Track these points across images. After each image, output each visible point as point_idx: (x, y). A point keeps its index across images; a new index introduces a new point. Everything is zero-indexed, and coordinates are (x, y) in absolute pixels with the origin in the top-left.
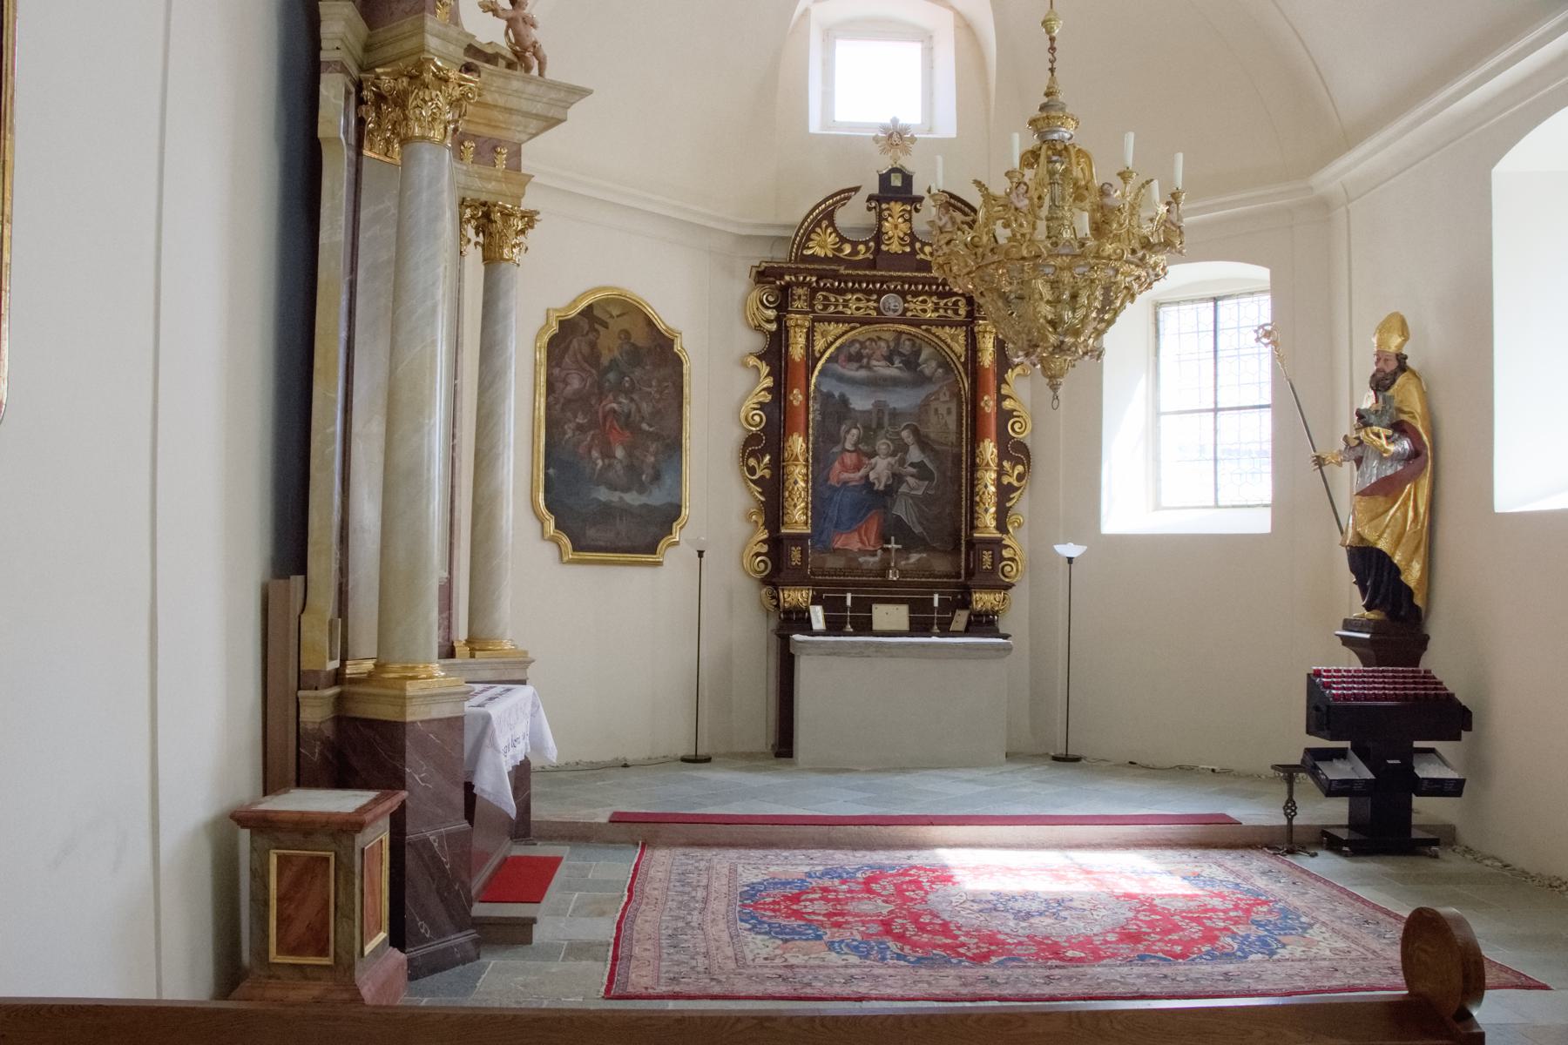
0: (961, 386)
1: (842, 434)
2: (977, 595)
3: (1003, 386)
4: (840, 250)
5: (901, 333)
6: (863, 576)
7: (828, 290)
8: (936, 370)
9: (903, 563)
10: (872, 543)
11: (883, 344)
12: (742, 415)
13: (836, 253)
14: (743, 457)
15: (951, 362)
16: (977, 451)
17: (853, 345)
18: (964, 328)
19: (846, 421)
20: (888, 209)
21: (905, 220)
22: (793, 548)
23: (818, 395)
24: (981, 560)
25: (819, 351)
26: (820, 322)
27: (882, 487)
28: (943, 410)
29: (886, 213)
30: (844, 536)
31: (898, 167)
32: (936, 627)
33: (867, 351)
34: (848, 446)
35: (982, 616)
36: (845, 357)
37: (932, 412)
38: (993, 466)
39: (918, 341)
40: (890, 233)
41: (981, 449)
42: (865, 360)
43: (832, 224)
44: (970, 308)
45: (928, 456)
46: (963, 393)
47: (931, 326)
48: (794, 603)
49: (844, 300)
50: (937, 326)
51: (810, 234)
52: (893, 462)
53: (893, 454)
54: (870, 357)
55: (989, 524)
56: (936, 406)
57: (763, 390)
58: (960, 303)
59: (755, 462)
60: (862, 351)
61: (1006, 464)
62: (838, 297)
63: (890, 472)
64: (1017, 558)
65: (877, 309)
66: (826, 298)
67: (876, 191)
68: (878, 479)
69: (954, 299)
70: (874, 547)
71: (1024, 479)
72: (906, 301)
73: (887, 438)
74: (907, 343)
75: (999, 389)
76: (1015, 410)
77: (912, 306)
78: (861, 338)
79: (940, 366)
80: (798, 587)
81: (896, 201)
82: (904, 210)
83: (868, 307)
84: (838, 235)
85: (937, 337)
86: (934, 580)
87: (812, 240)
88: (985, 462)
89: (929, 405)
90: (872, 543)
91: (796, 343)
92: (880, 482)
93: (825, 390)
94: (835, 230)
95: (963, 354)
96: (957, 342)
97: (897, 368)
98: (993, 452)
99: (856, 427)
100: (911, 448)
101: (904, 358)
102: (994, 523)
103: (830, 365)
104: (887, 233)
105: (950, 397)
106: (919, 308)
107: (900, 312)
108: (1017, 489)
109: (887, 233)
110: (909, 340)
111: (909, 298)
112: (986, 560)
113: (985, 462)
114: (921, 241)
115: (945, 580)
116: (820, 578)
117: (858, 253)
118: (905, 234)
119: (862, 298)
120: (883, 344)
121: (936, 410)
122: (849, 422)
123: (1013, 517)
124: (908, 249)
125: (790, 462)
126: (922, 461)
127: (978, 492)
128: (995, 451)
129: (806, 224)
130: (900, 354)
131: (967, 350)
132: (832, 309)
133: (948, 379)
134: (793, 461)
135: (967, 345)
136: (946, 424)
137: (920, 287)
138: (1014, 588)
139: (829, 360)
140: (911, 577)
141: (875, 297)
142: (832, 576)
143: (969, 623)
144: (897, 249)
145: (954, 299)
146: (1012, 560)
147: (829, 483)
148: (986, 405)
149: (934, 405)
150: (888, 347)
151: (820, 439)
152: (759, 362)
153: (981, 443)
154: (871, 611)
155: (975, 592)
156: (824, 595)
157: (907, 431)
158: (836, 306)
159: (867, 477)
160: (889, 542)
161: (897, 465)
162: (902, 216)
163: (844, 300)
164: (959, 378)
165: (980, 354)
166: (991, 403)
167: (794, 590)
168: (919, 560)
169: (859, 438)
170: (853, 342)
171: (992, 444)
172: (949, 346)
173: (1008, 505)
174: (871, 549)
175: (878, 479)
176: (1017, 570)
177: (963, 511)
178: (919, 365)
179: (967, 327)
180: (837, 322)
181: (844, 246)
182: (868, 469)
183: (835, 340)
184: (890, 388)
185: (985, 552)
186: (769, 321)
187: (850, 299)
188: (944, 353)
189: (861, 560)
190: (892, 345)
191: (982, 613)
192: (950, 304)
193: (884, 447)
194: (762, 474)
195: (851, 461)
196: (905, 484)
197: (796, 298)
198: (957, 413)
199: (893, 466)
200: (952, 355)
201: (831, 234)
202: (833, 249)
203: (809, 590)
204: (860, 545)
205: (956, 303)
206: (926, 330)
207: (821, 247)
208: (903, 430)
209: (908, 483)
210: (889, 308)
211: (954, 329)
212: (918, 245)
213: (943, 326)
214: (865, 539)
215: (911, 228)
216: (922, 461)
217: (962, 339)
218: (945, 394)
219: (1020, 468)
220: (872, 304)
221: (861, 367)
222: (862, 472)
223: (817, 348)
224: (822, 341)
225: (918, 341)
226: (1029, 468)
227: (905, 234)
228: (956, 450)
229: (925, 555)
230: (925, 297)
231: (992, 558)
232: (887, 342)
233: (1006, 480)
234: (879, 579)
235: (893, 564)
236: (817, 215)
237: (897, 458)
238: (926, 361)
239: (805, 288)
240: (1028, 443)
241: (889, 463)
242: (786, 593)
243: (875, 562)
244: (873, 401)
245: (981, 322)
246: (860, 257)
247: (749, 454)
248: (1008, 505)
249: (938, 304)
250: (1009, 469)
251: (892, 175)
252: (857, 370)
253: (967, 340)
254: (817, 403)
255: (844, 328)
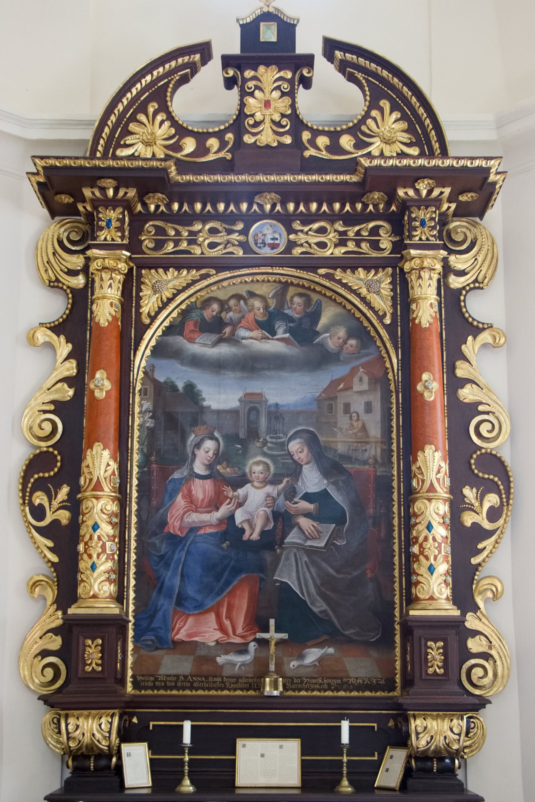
0: (388, 365)
1: (189, 450)
2: (419, 722)
3: (459, 363)
4: (177, 147)
5: (286, 285)
6: (222, 689)
7: (162, 216)
8: (345, 342)
9: (294, 664)
10: (239, 631)
11: (257, 304)
12: (25, 422)
13: (171, 153)
14: (23, 490)
15: (370, 328)
16: (414, 468)
17: (210, 306)
18: (390, 270)
19: (196, 429)
20: (255, 78)
21: (283, 94)
22: (89, 642)
23: (150, 388)
24: (425, 662)
25: (149, 314)
26: (150, 268)
27: (255, 536)
28: (358, 406)
29: (251, 84)
30: (191, 620)
31: (271, 10)
32: (345, 782)
33: (231, 314)
34: (199, 468)
35: (431, 759)
36: (195, 324)
37: (340, 408)
38: (442, 492)
39: (315, 297)
40: (259, 117)
41: (419, 463)
42: (228, 330)
43: (164, 108)
44: (398, 238)
45: (335, 484)
46: (390, 376)
47: (335, 269)
48: (87, 739)
49: (191, 233)
50: (344, 269)
51: (127, 125)
52: (275, 494)
53: (274, 481)
54: (235, 325)
55: (437, 595)
56: (347, 400)
57: (60, 381)
58: (381, 232)
59: (45, 498)
60: (223, 315)
61: (469, 493)
62: (179, 228)
63: (269, 511)
64: (493, 652)
65: (244, 245)
66: (160, 231)
67: (235, 49)
68: (249, 522)
69: (371, 225)
70: (243, 637)
71: (500, 516)
72: (290, 231)
73: (265, 455)
74: (297, 300)
75: (452, 369)
76: (481, 403)
77: (302, 238)
78: (222, 295)
79: (350, 335)
80: (94, 712)
81: (267, 65)
82: (281, 79)
83: (228, 242)
84: (174, 123)
85: (345, 286)
86: (348, 694)
87: (132, 133)
88: (427, 485)
89: (335, 398)
90: (239, 631)
91: (104, 298)
92: (252, 528)
93: (162, 380)
94: (170, 117)
95: (389, 311)
96: (378, 293)
97: (280, 340)
98: (440, 467)
99: (212, 438)
100: (306, 469)
101: (292, 325)
102: (447, 592)
103: (171, 339)
104: (252, 116)
105: (369, 383)
106: (313, 240)
107: (281, 248)
108: (490, 534)
109: (252, 116)
110: (300, 295)
111: (297, 225)
112: (434, 658)
113: (427, 485)
114: (310, 129)
115: (367, 694)
116: (150, 692)
117: (207, 151)
118: (283, 116)
119: (220, 229)
120: (257, 304)
121: (347, 408)
122: (201, 430)
123: (486, 581)
124: (288, 140)
125: (88, 494)
126: (325, 489)
127: (417, 538)
128: (445, 467)
129: (120, 107)
130: (289, 319)
131: (394, 306)
132: (170, 247)
133: (367, 355)
134: (94, 490)
135: (394, 298)
136: (364, 429)
137: (314, 206)
138: (488, 706)
139: (169, 331)
140: (307, 690)
141: (240, 226)
142: (171, 688)
143: (408, 772)
144: (269, 140)
145: (371, 225)
146: (486, 656)
147: (166, 530)
148: (426, 387)
149: (342, 399)
150: (266, 307)
151: (153, 458)
152: (55, 337)
153: (420, 454)
154: (233, 752)
155: (415, 717)
156: (151, 724)
157: (298, 440)
158: (177, 243)
159: (231, 518)
160: (266, 630)
161: (282, 497)
162: (278, 88)
163: (191, 233)
164: (383, 352)
165: (414, 306)
166: (435, 386)
167: (87, 717)
168: (320, 660)
169: (217, 453)
170: (207, 302)
171: (438, 455)
172: (363, 300)
173: (474, 561)
174: (238, 640)
175: (249, 522)
176: (495, 675)
177: (396, 573)
178: (318, 334)
179: (394, 268)
180: (179, 268)
181: (184, 141)
182: (231, 507)
183: (175, 296)
184: (268, 373)
185: (429, 643)
186: (72, 273)
187: (200, 231)
188: (358, 315)
189: (220, 660)
190: (272, 304)
191: (430, 754)
192: (365, 233)
193: (259, 468)
194: (54, 517)
195: (204, 492)
196: (295, 530)
197: (104, 224)
198: (382, 410)
199: (274, 499)
200: (370, 314)
201: (162, 123)
202: (166, 147)
203: (112, 716)
204: (218, 635)
205: (375, 231)
206: (328, 276)
207: (147, 144)
208: (290, 439)
209: (300, 529)
210: (264, 243)
211: (373, 272)
212: (306, 136)
213: (354, 269)
214: (227, 623)
215: (293, 106)
216: (325, 489)
217: (385, 287)
218: (361, 380)
219: (492, 499)
220: (235, 237)
221: (221, 340)
222: (224, 510)
223: (145, 310)
224: (154, 298)
225: (315, 297)
226: (508, 498)
227: (283, 116)
228: (380, 471)
229: (331, 650)
230: (322, 224)
231: (445, 654)
232: (263, 298)
233: (468, 519)
234: (251, 693)
235: (272, 668)
236: (140, 94)
237: (281, 486)
238: (327, 329)
239: (120, 210)
240: (506, 456)
241: (268, 496)
242: (72, 721)
243: (243, 664)
244: (241, 394)
245: (413, 252)
246: (211, 157)
247: (33, 484)
248: (474, 561)
249: (345, 233)
250: (473, 501)
251: (262, 24)
252: (215, 344)
253: (393, 290)
254: (147, 400)
255: (190, 278)
